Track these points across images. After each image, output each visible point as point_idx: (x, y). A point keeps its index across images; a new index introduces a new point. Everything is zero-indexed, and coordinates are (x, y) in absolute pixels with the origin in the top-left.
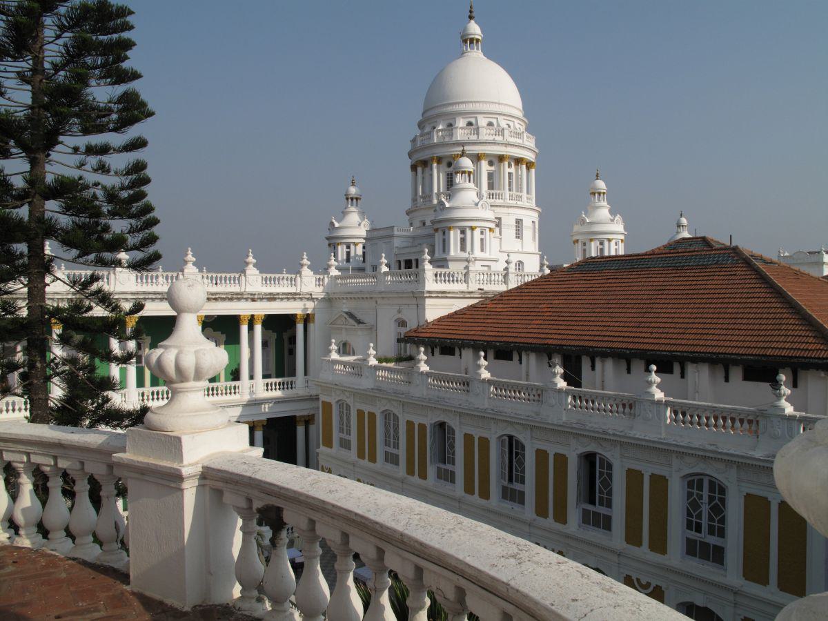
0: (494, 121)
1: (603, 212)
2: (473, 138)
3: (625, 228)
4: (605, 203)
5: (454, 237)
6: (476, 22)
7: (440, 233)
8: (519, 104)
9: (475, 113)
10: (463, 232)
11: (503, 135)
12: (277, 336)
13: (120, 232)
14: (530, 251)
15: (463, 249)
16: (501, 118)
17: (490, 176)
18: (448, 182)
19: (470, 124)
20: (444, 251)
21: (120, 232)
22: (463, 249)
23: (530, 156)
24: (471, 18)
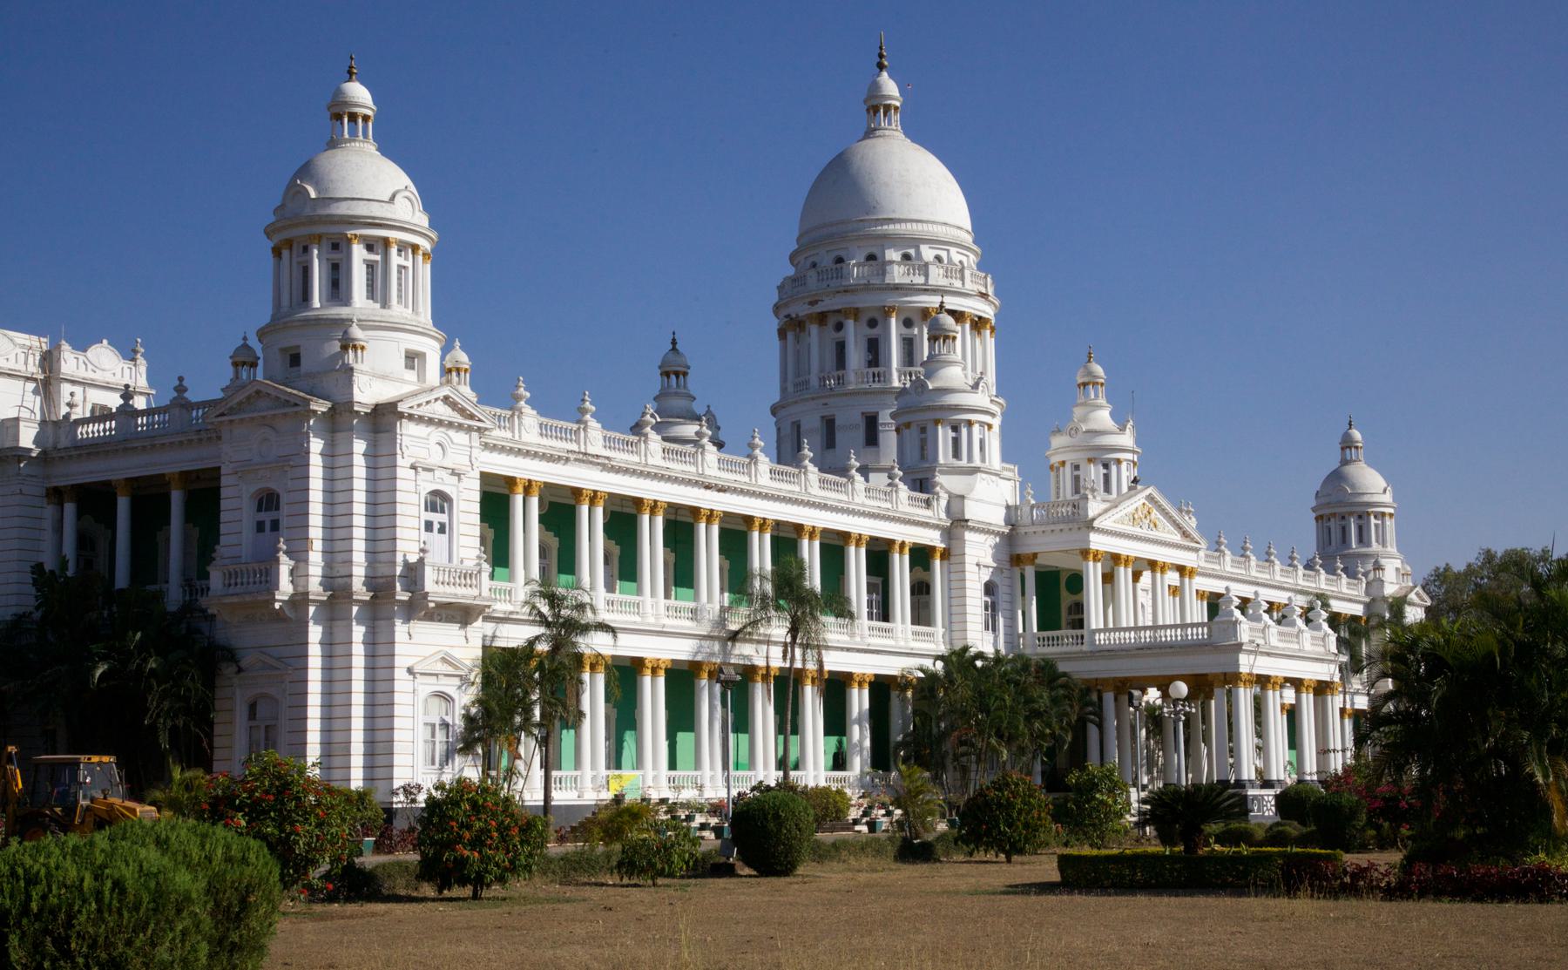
0: (944, 254)
1: (1103, 417)
2: (920, 280)
3: (1137, 442)
4: (1102, 401)
5: (944, 435)
6: (891, 76)
7: (914, 430)
8: (968, 225)
9: (916, 242)
10: (955, 429)
11: (963, 279)
12: (323, 633)
13: (367, 392)
14: (421, 430)
15: (957, 454)
16: (953, 250)
17: (371, 266)
18: (342, 270)
19: (906, 257)
20: (923, 457)
21: (367, 392)
22: (957, 454)
23: (987, 310)
24: (881, 67)
